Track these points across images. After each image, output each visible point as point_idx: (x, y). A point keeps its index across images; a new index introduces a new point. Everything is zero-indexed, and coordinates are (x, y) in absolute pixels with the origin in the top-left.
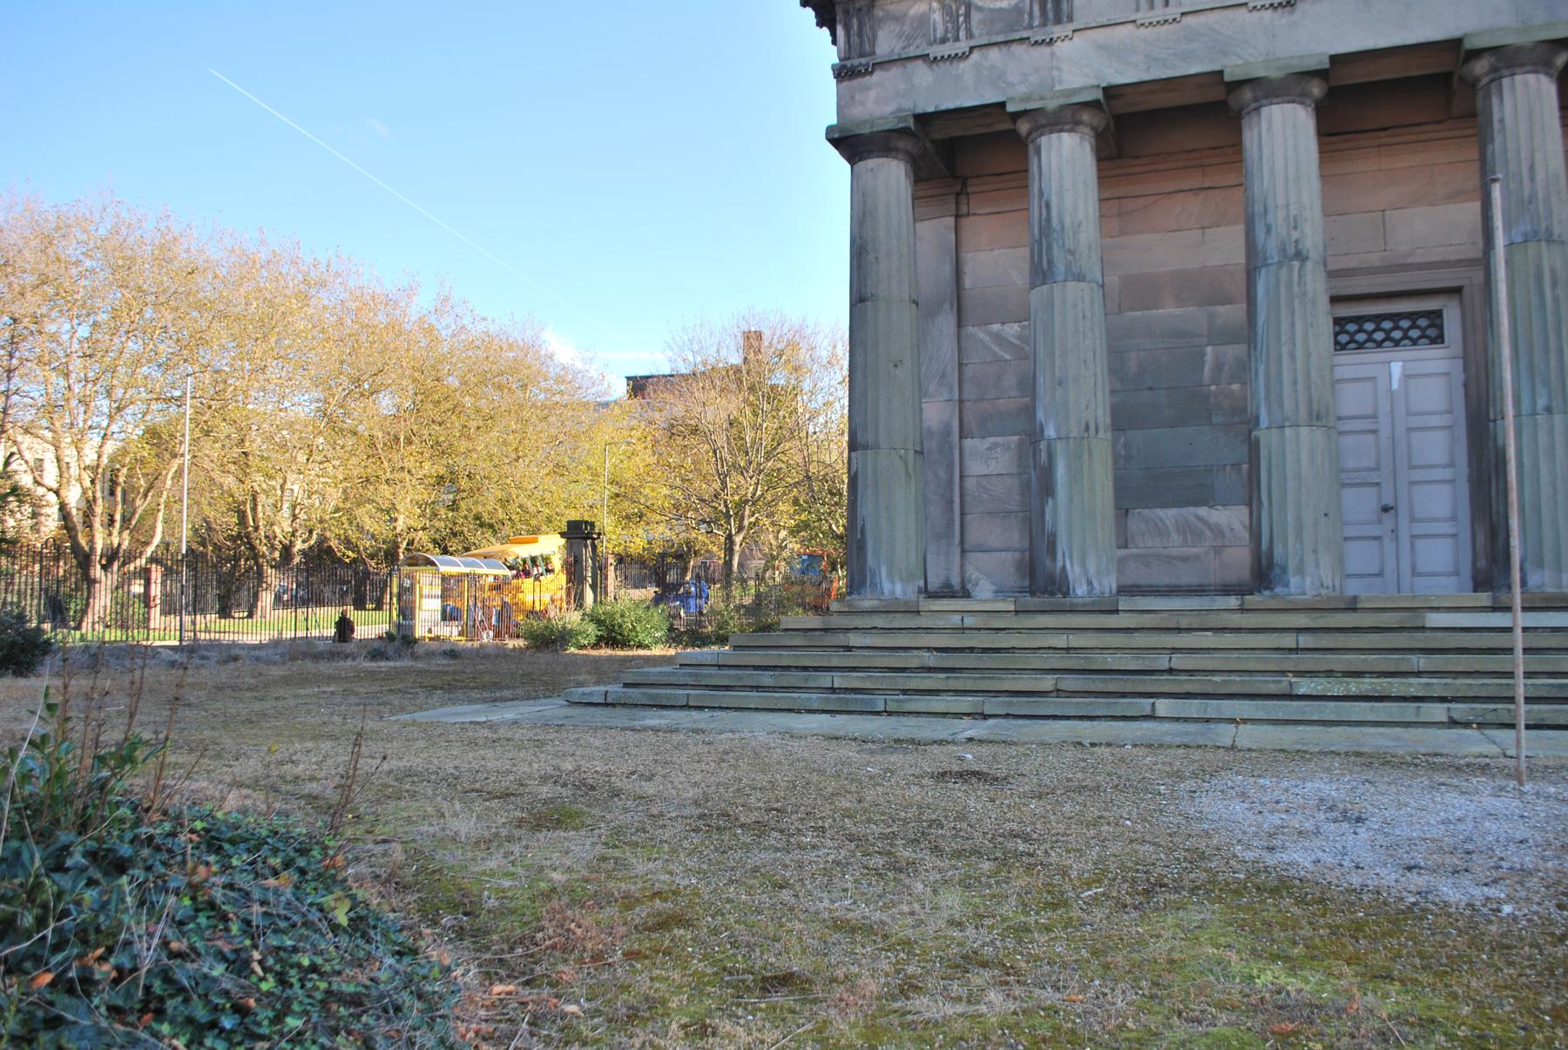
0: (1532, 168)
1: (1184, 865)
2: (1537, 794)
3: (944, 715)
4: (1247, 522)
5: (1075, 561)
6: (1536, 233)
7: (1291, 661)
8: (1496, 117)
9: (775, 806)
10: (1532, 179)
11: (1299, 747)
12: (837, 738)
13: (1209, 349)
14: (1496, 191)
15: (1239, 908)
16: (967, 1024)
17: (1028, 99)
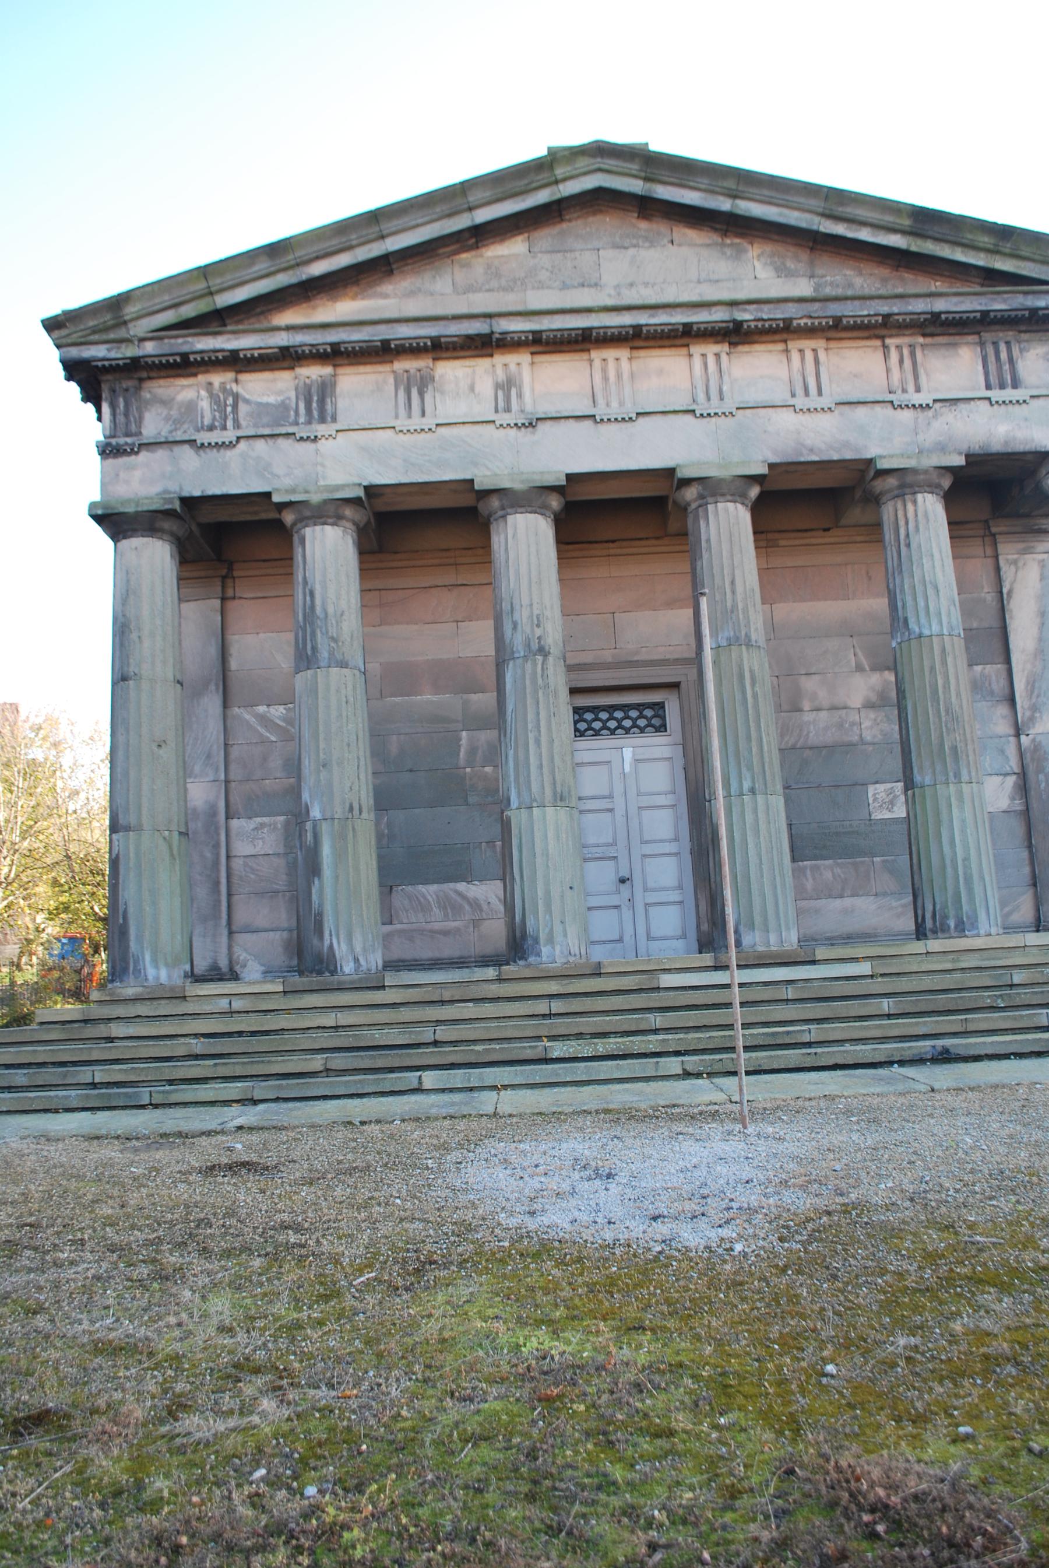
0: (733, 583)
1: (452, 1239)
2: (759, 1135)
3: (212, 1103)
4: (502, 897)
5: (342, 937)
6: (737, 638)
7: (546, 1027)
8: (703, 538)
9: (29, 1221)
10: (733, 592)
11: (554, 1109)
12: (98, 1138)
13: (464, 734)
14: (704, 602)
15: (504, 1276)
16: (240, 1438)
17: (293, 491)
